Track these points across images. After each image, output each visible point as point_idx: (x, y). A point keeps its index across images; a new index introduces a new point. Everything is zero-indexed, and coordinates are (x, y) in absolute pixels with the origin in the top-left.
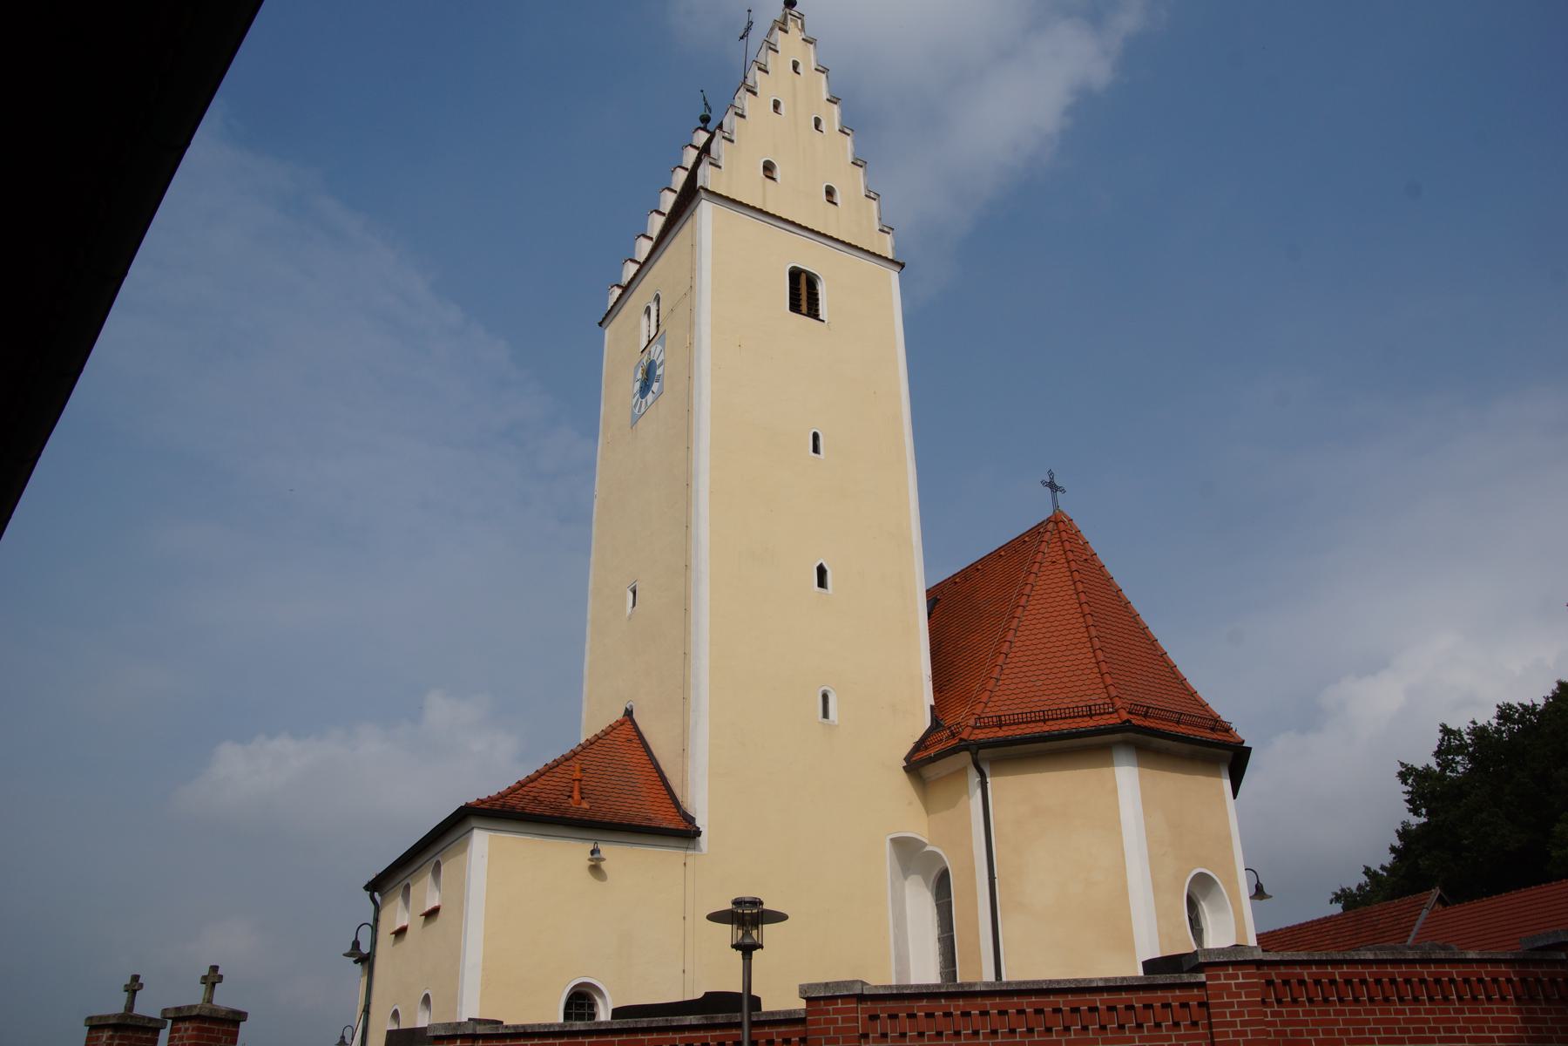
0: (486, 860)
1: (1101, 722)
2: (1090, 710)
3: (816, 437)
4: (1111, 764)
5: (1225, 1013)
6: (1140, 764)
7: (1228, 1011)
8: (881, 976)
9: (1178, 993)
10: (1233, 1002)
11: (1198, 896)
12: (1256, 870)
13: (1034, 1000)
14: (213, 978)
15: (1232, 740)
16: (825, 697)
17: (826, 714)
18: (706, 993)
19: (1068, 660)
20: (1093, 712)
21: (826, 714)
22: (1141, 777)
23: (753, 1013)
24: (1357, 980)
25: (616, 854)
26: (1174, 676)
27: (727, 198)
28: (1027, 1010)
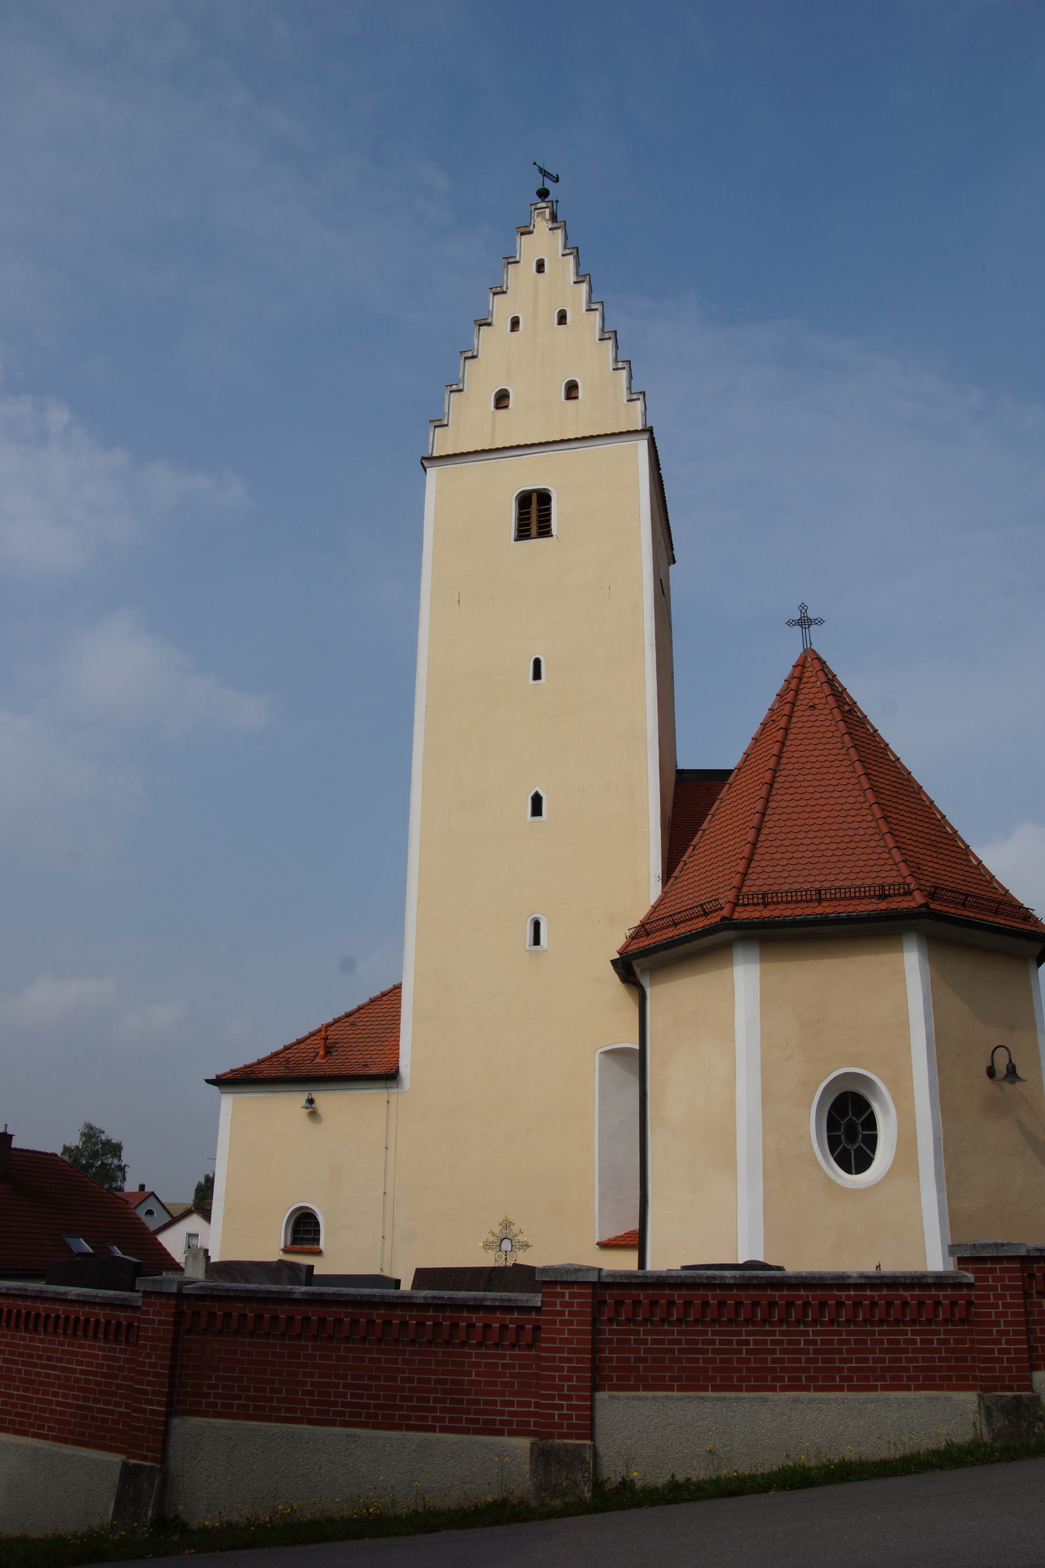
0: (230, 1117)
1: (829, 910)
2: (820, 894)
3: (537, 663)
4: (730, 963)
5: (732, 1377)
6: (762, 961)
7: (735, 1375)
8: (894, 1264)
9: (852, 1293)
10: (414, 1378)
11: (870, 1099)
12: (993, 1048)
13: (819, 1293)
14: (878, 1267)
15: (1038, 930)
16: (537, 925)
17: (537, 941)
18: (279, 1260)
19: (732, 797)
20: (823, 897)
21: (537, 941)
22: (763, 975)
23: (136, 1289)
24: (431, 1323)
25: (328, 1100)
26: (870, 776)
27: (455, 455)
28: (313, 1318)
